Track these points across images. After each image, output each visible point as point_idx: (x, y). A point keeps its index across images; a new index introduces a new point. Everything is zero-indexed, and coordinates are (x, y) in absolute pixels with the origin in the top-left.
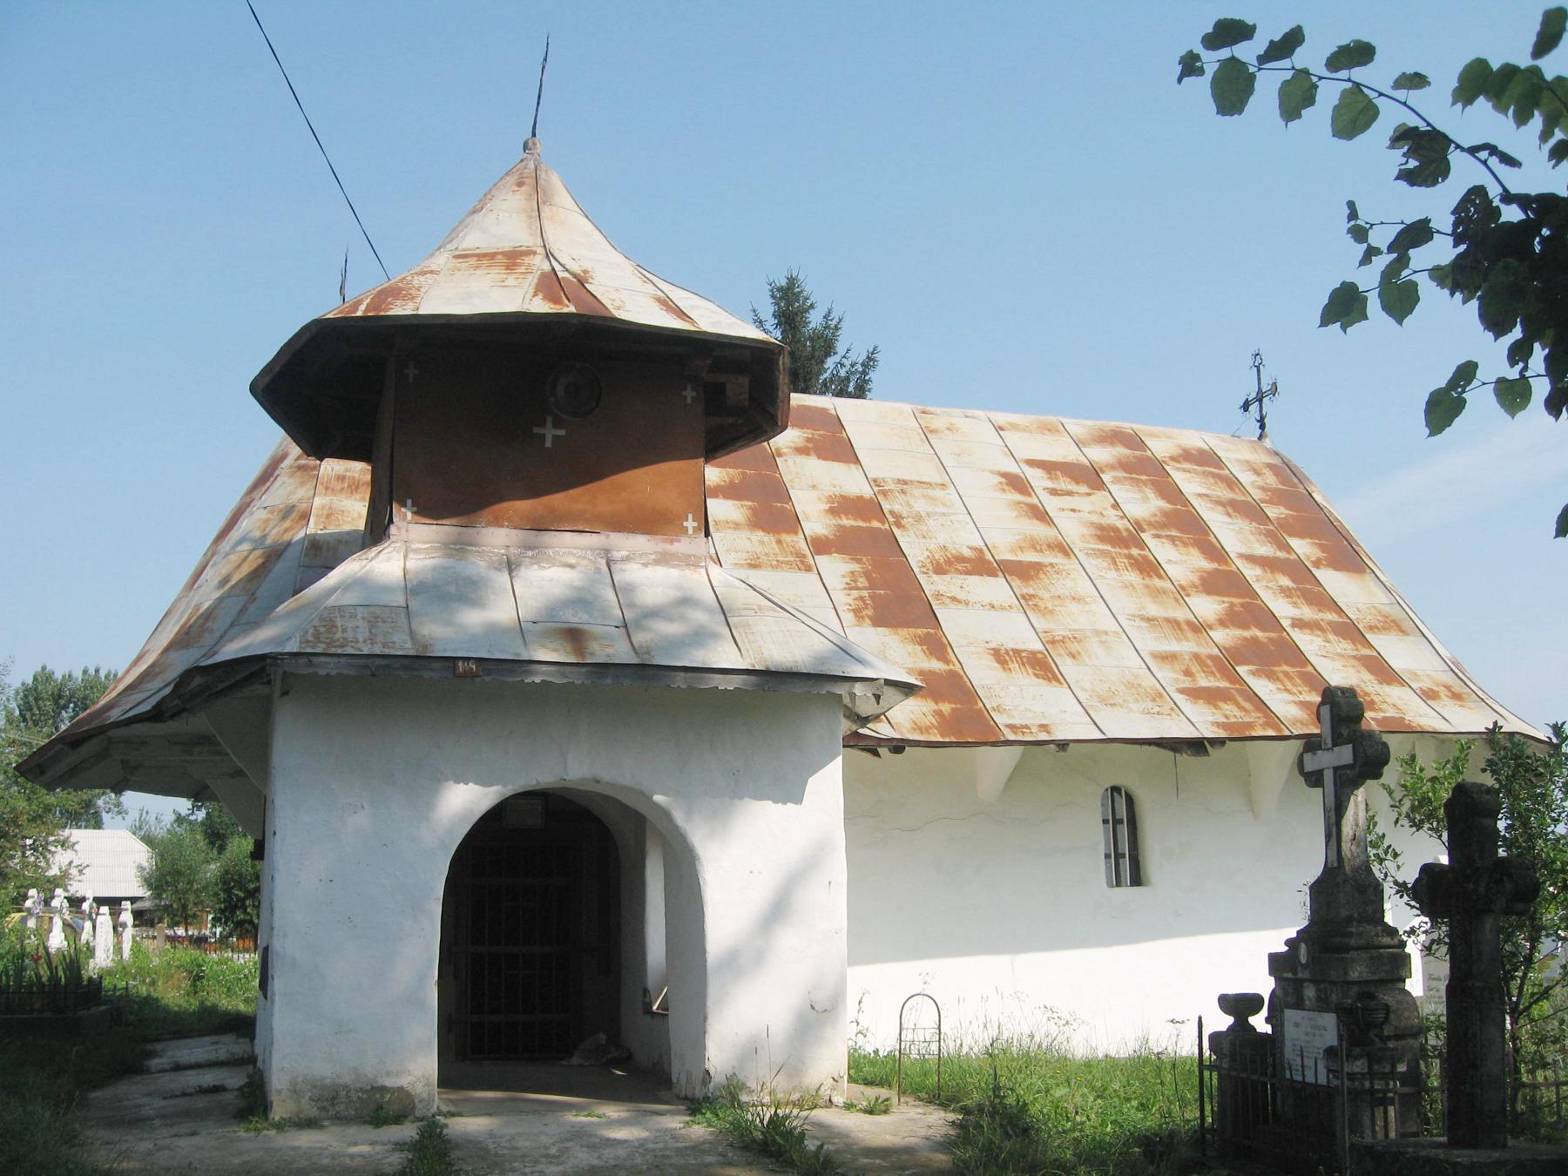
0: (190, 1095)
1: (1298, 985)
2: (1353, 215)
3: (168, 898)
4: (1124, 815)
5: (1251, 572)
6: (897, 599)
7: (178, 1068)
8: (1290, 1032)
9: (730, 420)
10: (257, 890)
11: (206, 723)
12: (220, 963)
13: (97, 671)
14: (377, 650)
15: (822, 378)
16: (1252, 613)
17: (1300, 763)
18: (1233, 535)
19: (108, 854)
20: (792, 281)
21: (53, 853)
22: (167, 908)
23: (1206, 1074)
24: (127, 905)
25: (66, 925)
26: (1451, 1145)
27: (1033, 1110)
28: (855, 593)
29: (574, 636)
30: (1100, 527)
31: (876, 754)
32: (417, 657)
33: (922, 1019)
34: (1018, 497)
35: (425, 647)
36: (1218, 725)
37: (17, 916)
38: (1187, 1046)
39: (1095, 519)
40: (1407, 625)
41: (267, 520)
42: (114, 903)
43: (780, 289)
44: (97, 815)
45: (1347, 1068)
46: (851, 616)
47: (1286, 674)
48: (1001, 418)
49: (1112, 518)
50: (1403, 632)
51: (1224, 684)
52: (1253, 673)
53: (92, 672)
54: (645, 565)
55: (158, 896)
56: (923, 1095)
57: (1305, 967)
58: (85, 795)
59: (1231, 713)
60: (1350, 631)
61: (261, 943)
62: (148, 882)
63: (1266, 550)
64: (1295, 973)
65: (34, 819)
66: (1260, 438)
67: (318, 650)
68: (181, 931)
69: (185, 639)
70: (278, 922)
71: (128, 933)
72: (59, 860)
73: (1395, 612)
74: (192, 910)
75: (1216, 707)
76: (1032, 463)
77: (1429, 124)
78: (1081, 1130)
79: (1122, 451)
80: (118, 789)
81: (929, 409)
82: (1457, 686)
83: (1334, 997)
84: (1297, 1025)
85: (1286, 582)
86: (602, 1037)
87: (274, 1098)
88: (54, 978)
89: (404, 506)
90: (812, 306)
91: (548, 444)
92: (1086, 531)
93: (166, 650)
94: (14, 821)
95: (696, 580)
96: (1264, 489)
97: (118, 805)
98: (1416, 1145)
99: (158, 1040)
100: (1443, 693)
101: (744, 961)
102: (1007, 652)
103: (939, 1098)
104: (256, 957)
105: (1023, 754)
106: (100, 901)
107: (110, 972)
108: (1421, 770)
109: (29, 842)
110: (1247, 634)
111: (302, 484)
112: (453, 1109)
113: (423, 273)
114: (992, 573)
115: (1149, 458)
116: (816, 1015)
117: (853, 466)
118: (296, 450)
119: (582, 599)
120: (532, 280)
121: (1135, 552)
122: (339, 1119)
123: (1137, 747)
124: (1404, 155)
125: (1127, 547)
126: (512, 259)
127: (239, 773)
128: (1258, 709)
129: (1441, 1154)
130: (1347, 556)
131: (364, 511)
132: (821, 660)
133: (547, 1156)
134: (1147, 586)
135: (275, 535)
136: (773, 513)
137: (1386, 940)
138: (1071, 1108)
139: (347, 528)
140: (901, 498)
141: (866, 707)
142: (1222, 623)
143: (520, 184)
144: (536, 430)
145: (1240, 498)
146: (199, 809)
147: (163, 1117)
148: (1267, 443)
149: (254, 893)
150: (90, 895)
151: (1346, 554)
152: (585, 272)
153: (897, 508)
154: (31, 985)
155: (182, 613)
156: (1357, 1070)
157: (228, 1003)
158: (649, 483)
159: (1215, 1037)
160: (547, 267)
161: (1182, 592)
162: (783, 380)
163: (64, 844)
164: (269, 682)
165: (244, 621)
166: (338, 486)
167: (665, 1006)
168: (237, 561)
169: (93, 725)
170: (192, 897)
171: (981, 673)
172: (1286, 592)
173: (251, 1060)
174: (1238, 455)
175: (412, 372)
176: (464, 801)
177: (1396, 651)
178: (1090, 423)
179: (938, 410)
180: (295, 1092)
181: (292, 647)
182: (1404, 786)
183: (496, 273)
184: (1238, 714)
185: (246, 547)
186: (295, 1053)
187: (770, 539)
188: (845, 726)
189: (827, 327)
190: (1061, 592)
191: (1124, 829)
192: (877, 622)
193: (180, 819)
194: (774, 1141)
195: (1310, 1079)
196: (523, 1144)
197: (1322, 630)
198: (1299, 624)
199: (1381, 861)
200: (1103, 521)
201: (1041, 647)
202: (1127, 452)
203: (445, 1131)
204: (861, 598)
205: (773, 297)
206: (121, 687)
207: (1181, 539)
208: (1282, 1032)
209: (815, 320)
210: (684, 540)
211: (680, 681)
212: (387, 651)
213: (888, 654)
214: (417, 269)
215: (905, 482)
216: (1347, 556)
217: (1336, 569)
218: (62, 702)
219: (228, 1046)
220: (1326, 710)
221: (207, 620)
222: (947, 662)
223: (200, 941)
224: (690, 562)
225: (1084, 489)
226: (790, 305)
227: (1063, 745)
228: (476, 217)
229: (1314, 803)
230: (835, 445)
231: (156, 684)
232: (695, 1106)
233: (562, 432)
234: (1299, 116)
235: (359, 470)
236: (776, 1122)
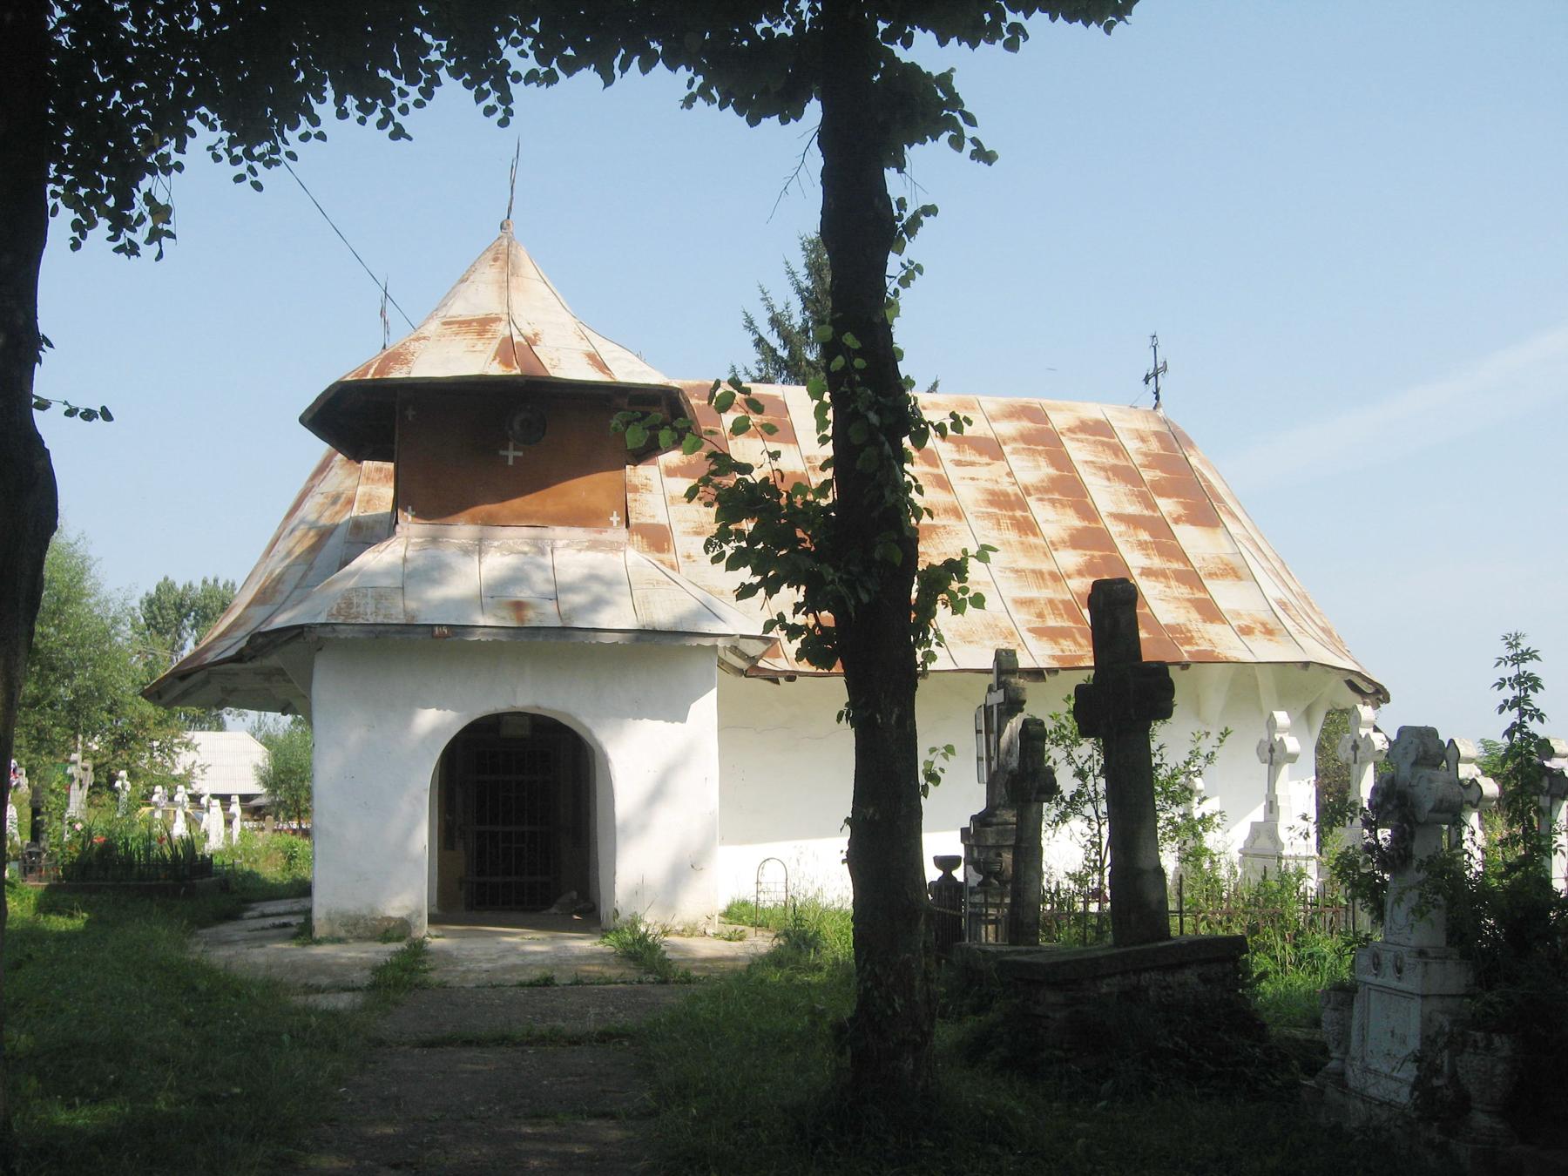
5: (1115, 529)
7: (264, 916)
13: (216, 581)
14: (379, 620)
22: (280, 804)
25: (186, 815)
29: (519, 606)
30: (993, 493)
31: (777, 682)
37: (146, 810)
39: (990, 486)
42: (225, 799)
49: (1006, 485)
50: (1239, 578)
53: (211, 582)
55: (273, 792)
60: (1191, 578)
62: (264, 781)
65: (160, 723)
72: (184, 760)
73: (1236, 561)
75: (1056, 643)
79: (1027, 425)
85: (1144, 536)
86: (574, 894)
87: (315, 923)
88: (175, 856)
91: (511, 462)
93: (248, 606)
94: (142, 725)
96: (1145, 455)
106: (214, 796)
109: (156, 744)
111: (350, 475)
113: (418, 339)
116: (685, 870)
117: (791, 446)
119: (517, 577)
120: (495, 345)
121: (1018, 513)
122: (359, 938)
126: (483, 325)
130: (1204, 511)
132: (682, 620)
135: (325, 521)
142: (1080, 573)
143: (495, 260)
144: (502, 453)
145: (1122, 463)
148: (1161, 412)
158: (585, 489)
168: (298, 543)
172: (1142, 545)
176: (435, 721)
177: (1223, 594)
178: (1003, 400)
180: (330, 920)
181: (322, 619)
183: (470, 339)
198: (1147, 572)
200: (996, 488)
207: (1060, 502)
218: (184, 611)
224: (614, 547)
225: (986, 459)
235: (390, 466)
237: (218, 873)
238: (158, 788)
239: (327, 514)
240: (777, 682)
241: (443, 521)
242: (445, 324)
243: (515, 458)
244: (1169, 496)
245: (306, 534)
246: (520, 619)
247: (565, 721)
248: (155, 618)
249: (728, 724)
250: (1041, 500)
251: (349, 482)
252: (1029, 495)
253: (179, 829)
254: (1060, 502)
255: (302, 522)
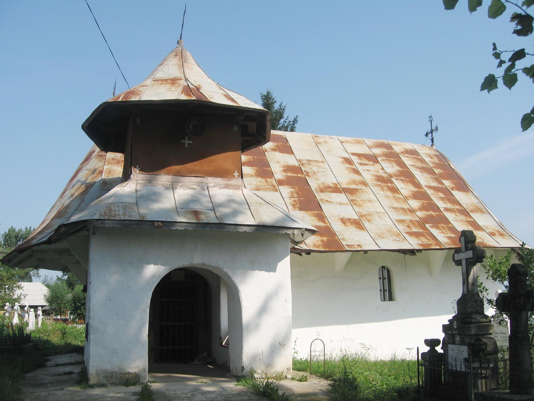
0: (61, 375)
1: (453, 336)
2: (495, 48)
3: (55, 305)
4: (385, 278)
5: (430, 192)
6: (308, 201)
7: (57, 365)
8: (450, 352)
9: (250, 138)
10: (85, 303)
11: (67, 244)
12: (72, 328)
13: (30, 228)
14: (127, 218)
15: (279, 126)
16: (430, 206)
17: (453, 256)
18: (423, 179)
19: (34, 290)
20: (268, 93)
21: (15, 290)
22: (54, 309)
23: (420, 367)
24: (40, 308)
25: (19, 315)
26: (511, 393)
27: (358, 380)
28: (293, 199)
29: (196, 213)
30: (377, 176)
31: (301, 255)
32: (140, 221)
33: (318, 347)
34: (349, 166)
35: (143, 217)
36: (419, 245)
38: (412, 356)
39: (376, 173)
40: (484, 210)
41: (88, 174)
42: (35, 307)
43: (264, 96)
44: (30, 277)
45: (472, 365)
46: (291, 207)
47: (442, 227)
48: (343, 139)
49: (381, 173)
51: (421, 230)
52: (431, 227)
54: (221, 188)
55: (51, 305)
56: (318, 374)
57: (456, 329)
58: (27, 270)
59: (424, 240)
60: (464, 212)
61: (86, 322)
62: (48, 300)
63: (435, 184)
64: (452, 332)
65: (8, 279)
66: (432, 145)
67: (106, 218)
68: (59, 317)
69: (59, 215)
70: (92, 314)
71: (40, 318)
72: (17, 293)
73: (480, 206)
74: (63, 310)
75: (419, 238)
76: (353, 154)
77: (525, 12)
78: (375, 387)
79: (384, 150)
80: (37, 267)
81: (317, 135)
82: (502, 231)
83: (467, 340)
84: (453, 350)
85: (442, 195)
86: (205, 354)
87: (90, 376)
88: (14, 334)
89: (136, 167)
90: (275, 102)
91: (186, 146)
92: (372, 178)
95: (237, 194)
96: (433, 163)
97: (38, 274)
98: (500, 393)
99: (49, 355)
100: (497, 233)
101: (256, 326)
102: (346, 219)
103: (325, 376)
104: (84, 326)
105: (351, 256)
106: (31, 307)
107: (34, 331)
108: (495, 260)
109: (7, 286)
110: (429, 213)
111: (100, 161)
112: (153, 380)
113: (142, 86)
114: (340, 192)
115: (394, 153)
116: (278, 346)
117: (291, 155)
118: (98, 149)
119: (194, 200)
120: (181, 89)
121: (389, 185)
122: (113, 384)
123: (392, 252)
124: (516, 24)
125: (387, 183)
126: (174, 81)
127: (78, 262)
128: (433, 239)
129: (508, 397)
130: (463, 186)
131: (122, 171)
132: (279, 221)
133: (187, 397)
134: (394, 197)
136: (264, 170)
137: (484, 320)
138: (371, 379)
139: (116, 176)
140: (308, 166)
141: (297, 239)
142: (420, 209)
143: (176, 56)
144: (182, 141)
146: (65, 275)
147: (51, 383)
148: (434, 147)
149: (84, 304)
150: (27, 305)
151: (462, 186)
152: (199, 86)
153: (307, 169)
154: (6, 336)
155: (58, 207)
156: (476, 366)
157: (75, 342)
158: (222, 159)
159: (423, 354)
160: (186, 84)
161: (406, 199)
162: (268, 124)
163: (19, 287)
164: (88, 230)
165: (78, 209)
166: (113, 162)
167: (227, 343)
168: (76, 190)
169: (27, 245)
170: (63, 305)
171: (337, 227)
172: (442, 199)
173: (83, 362)
174: (424, 151)
175: (138, 121)
176: (153, 271)
177: (480, 219)
178: (373, 140)
179: (320, 136)
180: (98, 374)
181: (96, 217)
182: (490, 266)
183: (168, 86)
184: (426, 241)
185: (79, 184)
186: (97, 361)
187: (262, 180)
188: (291, 245)
189: (280, 109)
190: (364, 199)
191: (386, 281)
192: (301, 209)
193: (58, 279)
194: (267, 391)
195: (459, 369)
196: (178, 392)
197: (455, 212)
198: (447, 210)
199: (482, 292)
200: (378, 174)
201: (357, 218)
202: (386, 150)
203: (151, 388)
204: (295, 201)
205: (262, 98)
206: (37, 232)
208: (448, 353)
209: (276, 106)
210: (234, 180)
211: (232, 229)
212: (130, 219)
213: (304, 220)
214: (140, 85)
215: (310, 161)
216: (463, 186)
217: (459, 190)
218: (18, 239)
219: (75, 357)
220: (463, 239)
221: (67, 208)
222: (325, 223)
223: (65, 321)
224: (237, 187)
225: (371, 163)
226: (268, 100)
227: (366, 252)
228: (161, 67)
229: (458, 272)
230: (285, 148)
231: (49, 231)
232: (238, 378)
233: (191, 142)
234: (476, 10)
235: (120, 156)
236: (268, 385)
237: (33, 341)
238: (7, 304)
239: (90, 178)
240: (301, 255)
241: (153, 173)
242: (154, 81)
243: (189, 144)
244: (447, 180)
245: (80, 187)
246: (197, 218)
247: (215, 271)
248: (7, 241)
249: (297, 276)
250: (397, 179)
251: (100, 164)
252: (392, 177)
253: (16, 320)
254: (405, 180)
255: (78, 182)
